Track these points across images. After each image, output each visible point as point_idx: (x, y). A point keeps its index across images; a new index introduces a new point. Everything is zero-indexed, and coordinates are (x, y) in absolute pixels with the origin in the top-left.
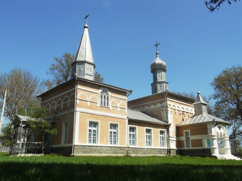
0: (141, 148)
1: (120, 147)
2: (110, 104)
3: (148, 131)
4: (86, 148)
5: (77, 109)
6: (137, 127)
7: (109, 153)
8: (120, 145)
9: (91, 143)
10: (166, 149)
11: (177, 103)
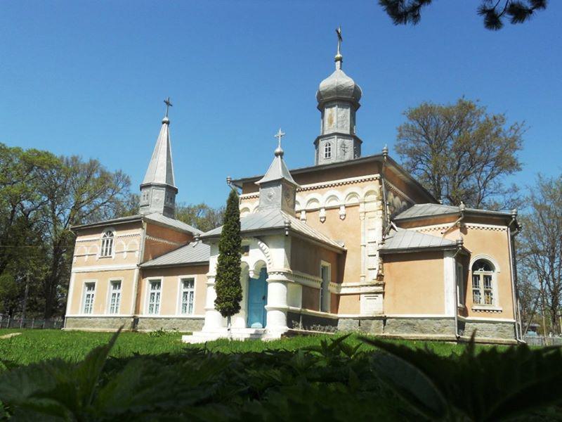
0: (166, 319)
1: (120, 318)
2: (113, 251)
3: (188, 283)
4: (77, 321)
5: (74, 269)
6: (162, 278)
7: (105, 327)
8: (120, 313)
9: (204, 319)
10: (511, 323)
11: (321, 187)
